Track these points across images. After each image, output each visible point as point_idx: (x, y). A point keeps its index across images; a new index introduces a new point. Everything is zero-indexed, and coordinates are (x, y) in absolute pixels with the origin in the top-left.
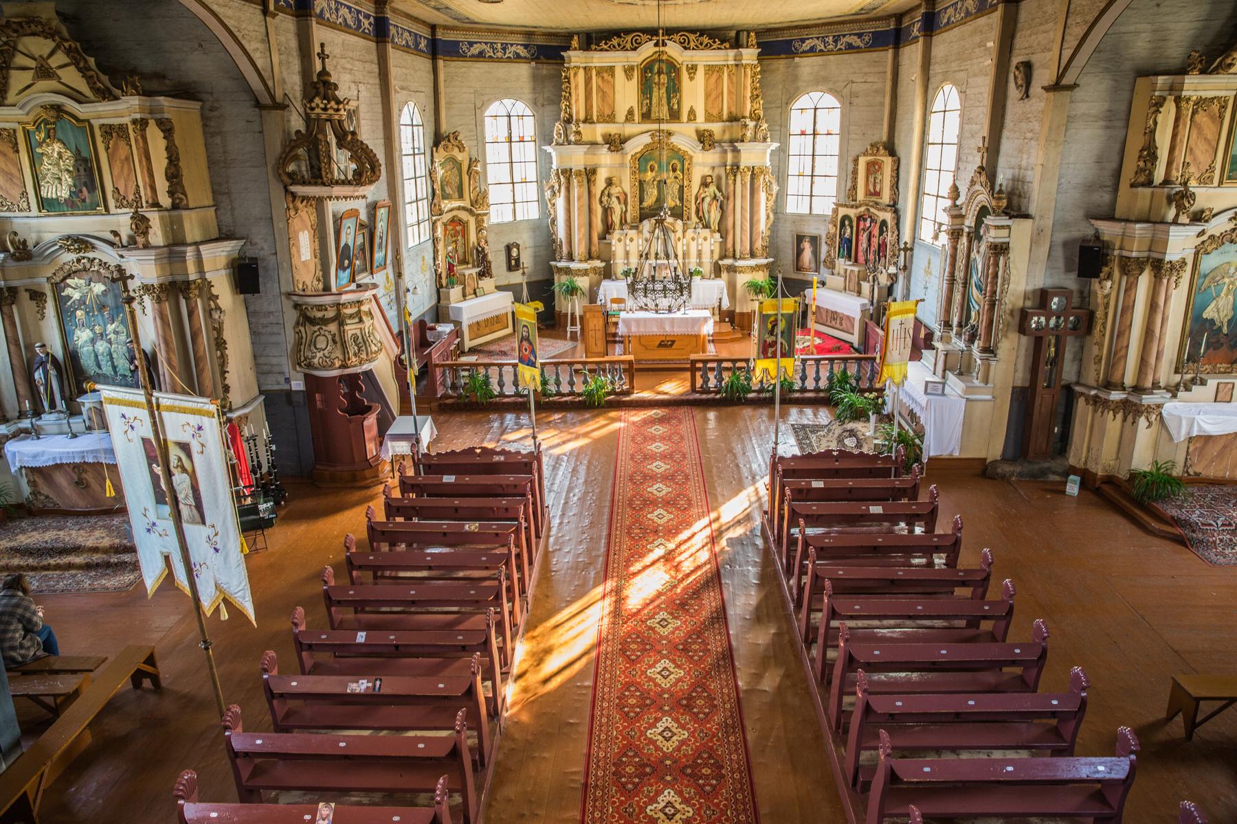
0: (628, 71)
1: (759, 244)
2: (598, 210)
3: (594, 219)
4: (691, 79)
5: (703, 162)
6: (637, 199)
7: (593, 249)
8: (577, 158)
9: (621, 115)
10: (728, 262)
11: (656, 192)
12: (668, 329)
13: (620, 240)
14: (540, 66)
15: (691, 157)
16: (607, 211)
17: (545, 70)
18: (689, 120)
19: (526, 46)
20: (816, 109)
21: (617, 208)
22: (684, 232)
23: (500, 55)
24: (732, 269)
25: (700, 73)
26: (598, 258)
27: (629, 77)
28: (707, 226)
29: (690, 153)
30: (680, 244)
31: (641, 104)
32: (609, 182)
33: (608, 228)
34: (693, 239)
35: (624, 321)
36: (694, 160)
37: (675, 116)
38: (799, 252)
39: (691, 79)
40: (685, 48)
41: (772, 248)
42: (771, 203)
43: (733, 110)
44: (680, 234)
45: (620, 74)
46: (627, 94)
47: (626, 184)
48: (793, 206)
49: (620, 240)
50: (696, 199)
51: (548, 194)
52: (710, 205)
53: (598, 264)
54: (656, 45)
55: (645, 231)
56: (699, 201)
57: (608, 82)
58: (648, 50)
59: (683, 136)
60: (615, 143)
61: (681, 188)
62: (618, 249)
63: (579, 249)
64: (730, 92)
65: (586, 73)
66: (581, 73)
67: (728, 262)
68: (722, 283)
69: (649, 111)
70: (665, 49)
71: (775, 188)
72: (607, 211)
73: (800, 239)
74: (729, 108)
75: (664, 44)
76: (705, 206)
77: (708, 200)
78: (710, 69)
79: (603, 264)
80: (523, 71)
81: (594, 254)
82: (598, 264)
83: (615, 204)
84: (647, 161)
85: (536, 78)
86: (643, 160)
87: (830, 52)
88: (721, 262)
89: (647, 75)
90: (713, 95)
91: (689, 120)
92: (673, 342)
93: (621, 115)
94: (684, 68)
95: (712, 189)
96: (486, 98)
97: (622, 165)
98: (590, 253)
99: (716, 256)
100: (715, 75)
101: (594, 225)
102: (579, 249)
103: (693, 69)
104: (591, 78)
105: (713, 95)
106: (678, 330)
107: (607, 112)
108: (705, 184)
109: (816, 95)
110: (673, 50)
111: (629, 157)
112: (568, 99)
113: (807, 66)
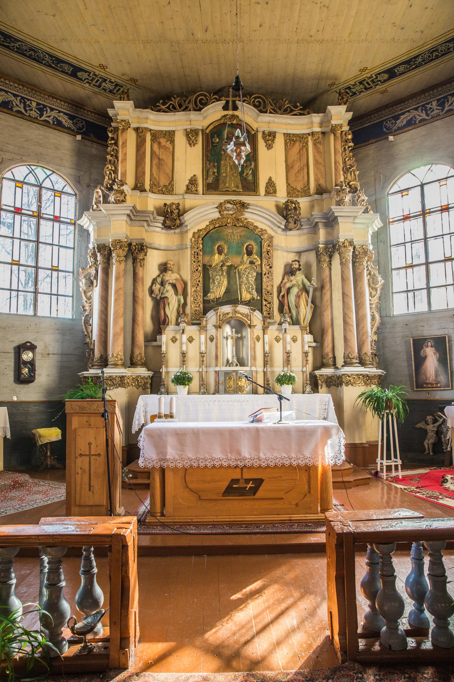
0: (191, 135)
1: (368, 349)
2: (149, 304)
3: (140, 312)
4: (269, 147)
5: (287, 245)
6: (200, 288)
7: (137, 352)
8: (117, 227)
9: (181, 183)
10: (328, 371)
11: (225, 283)
12: (246, 452)
13: (174, 340)
14: (87, 142)
15: (271, 238)
16: (159, 303)
17: (94, 149)
18: (268, 193)
19: (71, 117)
20: (422, 186)
21: (173, 301)
22: (265, 329)
23: (33, 114)
24: (335, 383)
25: (280, 142)
26: (144, 365)
27: (192, 143)
28: (295, 322)
29: (270, 232)
30: (259, 345)
31: (206, 172)
32: (164, 268)
33: (160, 323)
34: (277, 340)
35: (152, 435)
36: (276, 242)
37: (250, 186)
38: (420, 361)
39: (269, 147)
40: (261, 111)
41: (381, 357)
42: (375, 300)
43: (322, 182)
44: (258, 331)
45: (180, 140)
46: (189, 161)
47: (186, 271)
48: (399, 307)
49: (174, 340)
50: (279, 291)
51: (83, 283)
52: (298, 296)
53: (142, 372)
54: (225, 108)
55: (210, 327)
56: (284, 293)
57: (165, 148)
58: (214, 113)
59: (261, 212)
60: (172, 218)
61: (260, 276)
62: (172, 352)
63: (116, 348)
64: (316, 162)
65: (138, 136)
66: (131, 138)
67: (328, 371)
68: (324, 397)
69: (217, 180)
70: (236, 113)
71: (381, 281)
72: (159, 303)
73: (419, 344)
74: (316, 180)
75: (235, 108)
76: (292, 298)
77: (295, 291)
78: (291, 139)
79: (150, 373)
80: (65, 143)
81: (137, 358)
82: (142, 372)
83: (170, 293)
84: (214, 241)
85: (79, 154)
86: (209, 238)
87: (436, 118)
88: (317, 373)
89: (213, 142)
90: (297, 167)
91: (268, 193)
92: (259, 482)
93: (181, 183)
94: (260, 136)
95: (300, 277)
96: (7, 156)
97: (181, 248)
98: (131, 359)
99: (309, 368)
100: (297, 146)
101: (140, 318)
102: (116, 348)
103: (270, 137)
104: (144, 141)
105: (297, 167)
106: (269, 455)
107: (163, 181)
108: (290, 271)
109: (422, 172)
110: (247, 114)
111: (190, 235)
112: (115, 165)
113: (403, 142)
